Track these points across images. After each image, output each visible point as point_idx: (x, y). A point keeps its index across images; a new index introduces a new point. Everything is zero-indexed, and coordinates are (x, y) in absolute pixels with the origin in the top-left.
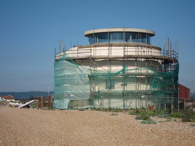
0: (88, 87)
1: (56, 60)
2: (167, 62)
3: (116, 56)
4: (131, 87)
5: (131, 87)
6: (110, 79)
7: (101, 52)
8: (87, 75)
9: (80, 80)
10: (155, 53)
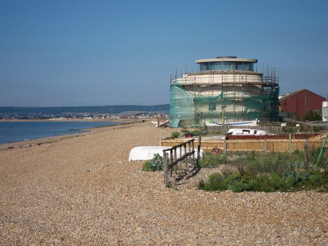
0: (193, 109)
4: (230, 109)
5: (230, 109)
6: (212, 102)
8: (192, 99)
9: (187, 104)
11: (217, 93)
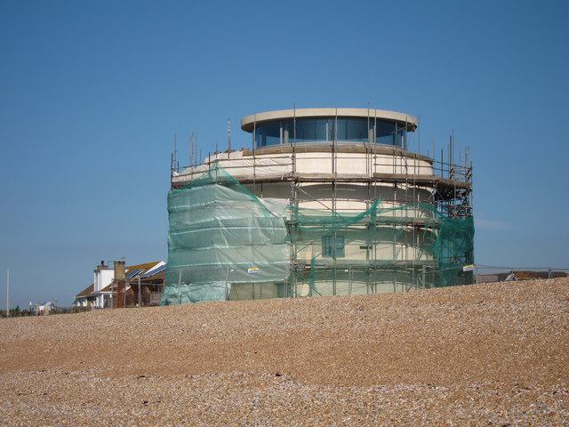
0: (286, 251)
1: (173, 183)
2: (446, 191)
3: (356, 175)
4: (384, 252)
5: (384, 252)
6: (334, 233)
7: (313, 164)
8: (282, 222)
9: (261, 234)
10: (425, 171)
11: (351, 207)
